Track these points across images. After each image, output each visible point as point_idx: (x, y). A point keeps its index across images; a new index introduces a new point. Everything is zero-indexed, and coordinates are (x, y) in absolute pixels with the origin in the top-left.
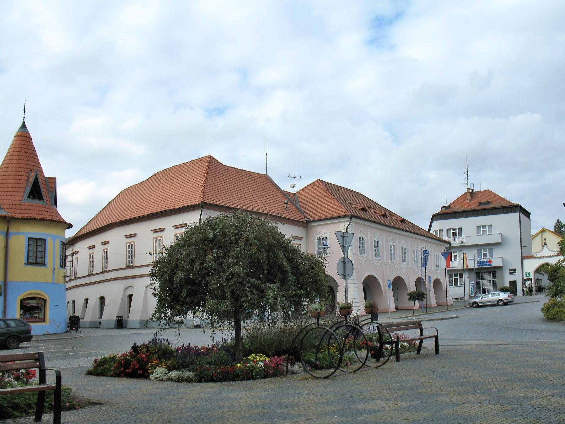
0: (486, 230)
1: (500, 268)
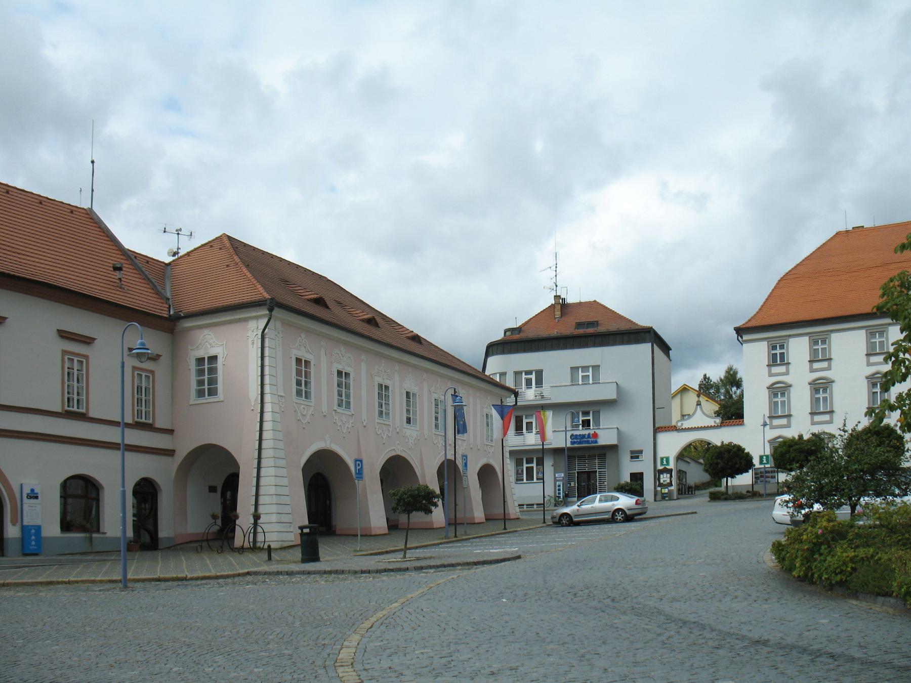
0: (589, 376)
1: (613, 448)
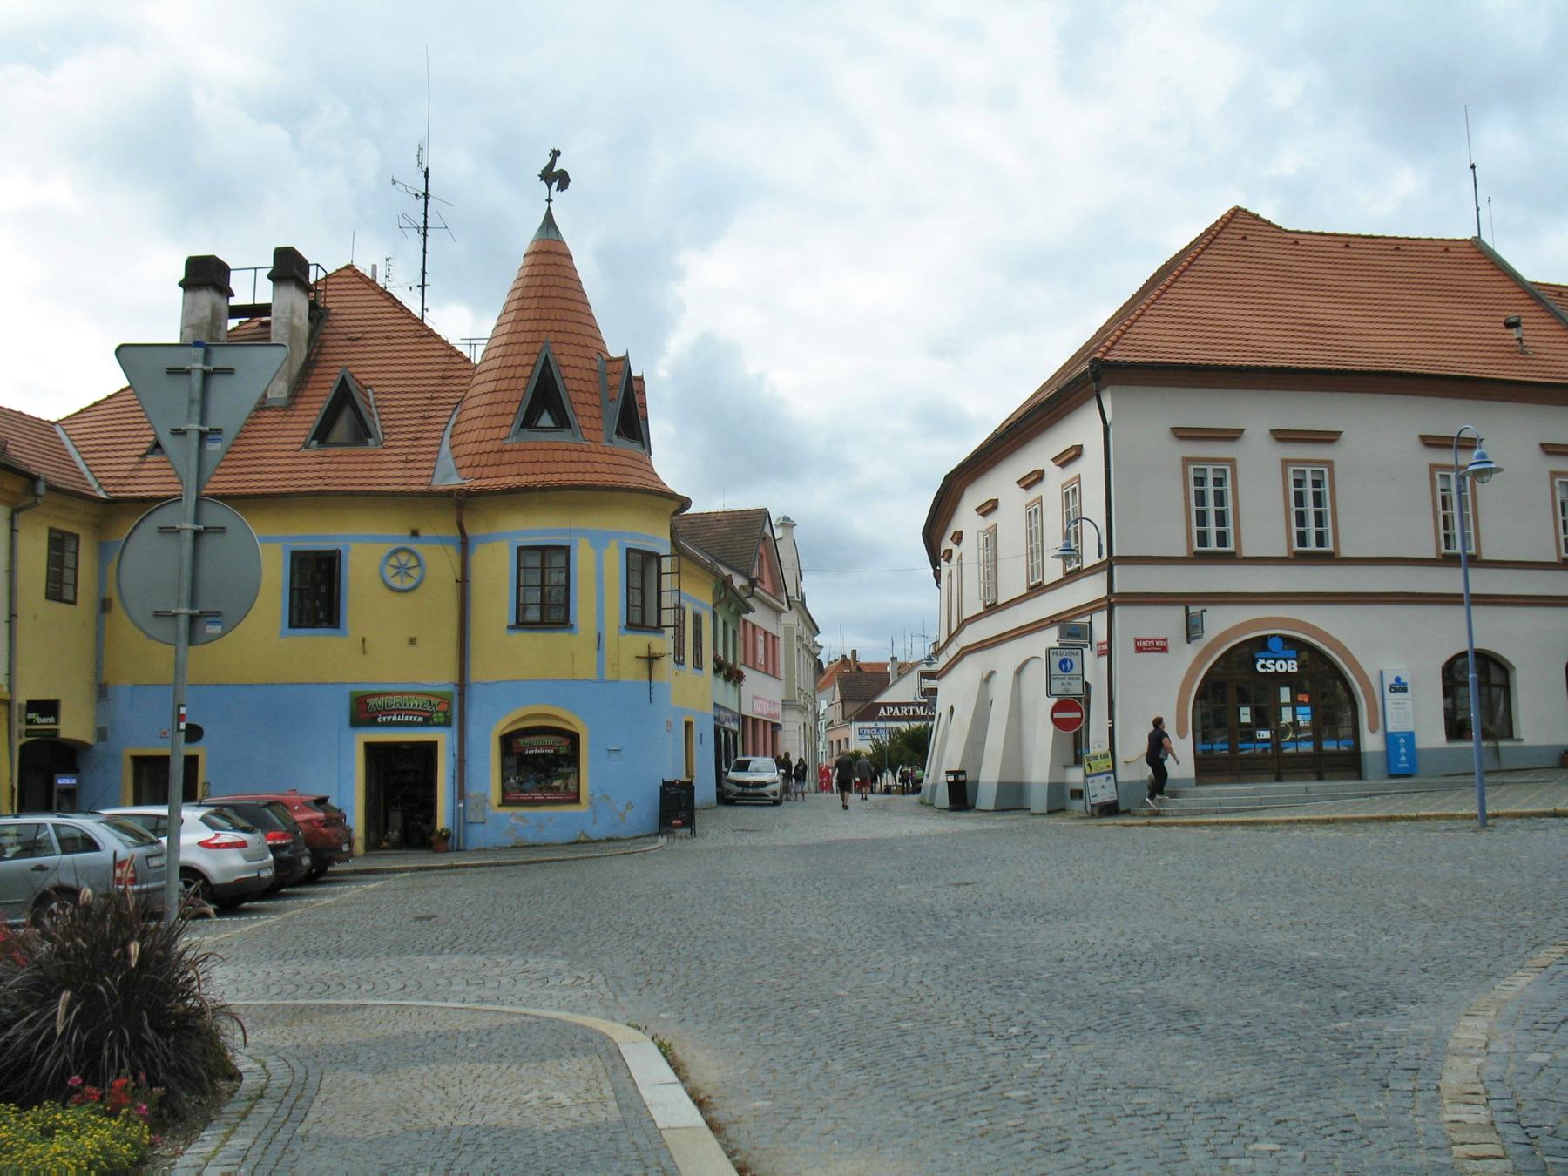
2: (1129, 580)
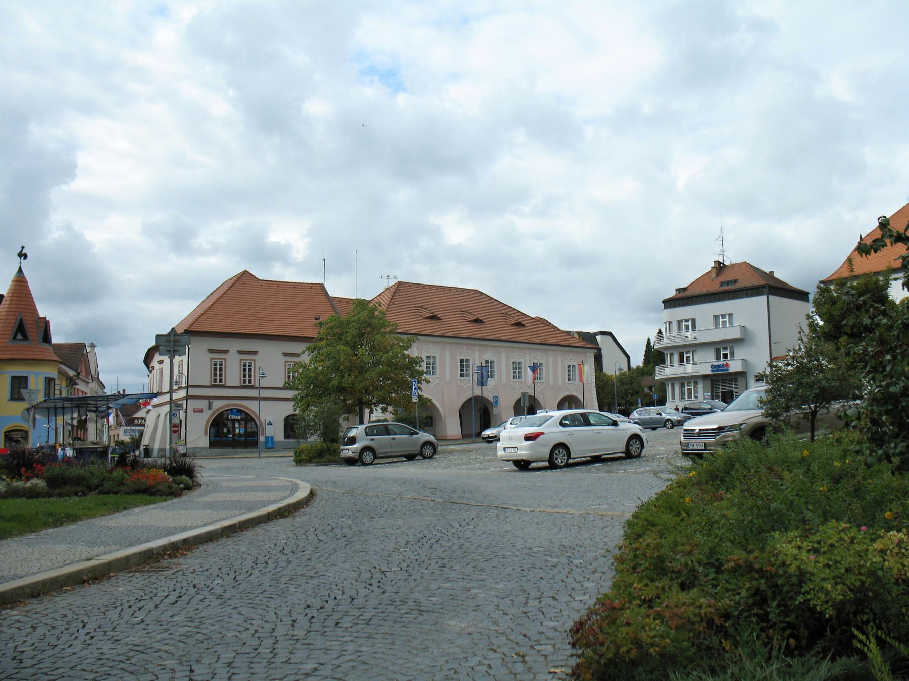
0: (726, 321)
1: (743, 374)
2: (192, 392)
